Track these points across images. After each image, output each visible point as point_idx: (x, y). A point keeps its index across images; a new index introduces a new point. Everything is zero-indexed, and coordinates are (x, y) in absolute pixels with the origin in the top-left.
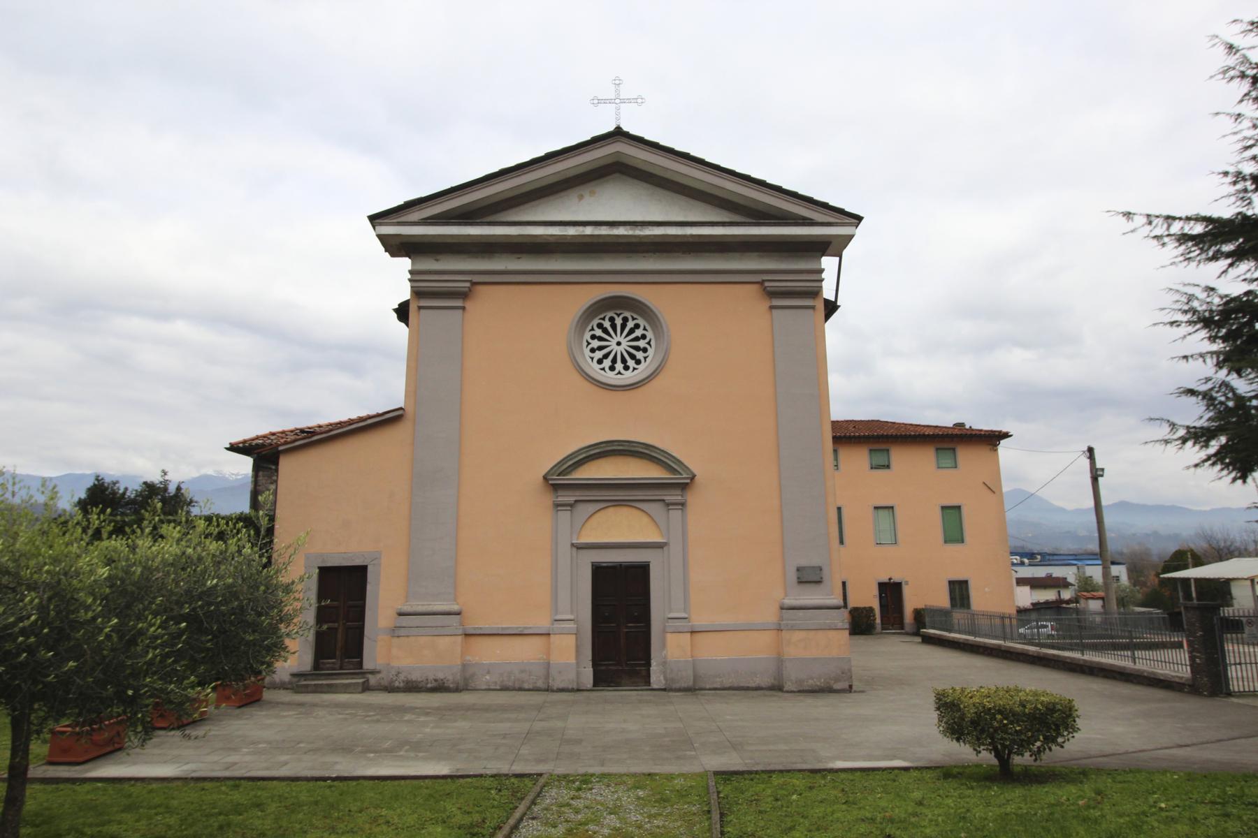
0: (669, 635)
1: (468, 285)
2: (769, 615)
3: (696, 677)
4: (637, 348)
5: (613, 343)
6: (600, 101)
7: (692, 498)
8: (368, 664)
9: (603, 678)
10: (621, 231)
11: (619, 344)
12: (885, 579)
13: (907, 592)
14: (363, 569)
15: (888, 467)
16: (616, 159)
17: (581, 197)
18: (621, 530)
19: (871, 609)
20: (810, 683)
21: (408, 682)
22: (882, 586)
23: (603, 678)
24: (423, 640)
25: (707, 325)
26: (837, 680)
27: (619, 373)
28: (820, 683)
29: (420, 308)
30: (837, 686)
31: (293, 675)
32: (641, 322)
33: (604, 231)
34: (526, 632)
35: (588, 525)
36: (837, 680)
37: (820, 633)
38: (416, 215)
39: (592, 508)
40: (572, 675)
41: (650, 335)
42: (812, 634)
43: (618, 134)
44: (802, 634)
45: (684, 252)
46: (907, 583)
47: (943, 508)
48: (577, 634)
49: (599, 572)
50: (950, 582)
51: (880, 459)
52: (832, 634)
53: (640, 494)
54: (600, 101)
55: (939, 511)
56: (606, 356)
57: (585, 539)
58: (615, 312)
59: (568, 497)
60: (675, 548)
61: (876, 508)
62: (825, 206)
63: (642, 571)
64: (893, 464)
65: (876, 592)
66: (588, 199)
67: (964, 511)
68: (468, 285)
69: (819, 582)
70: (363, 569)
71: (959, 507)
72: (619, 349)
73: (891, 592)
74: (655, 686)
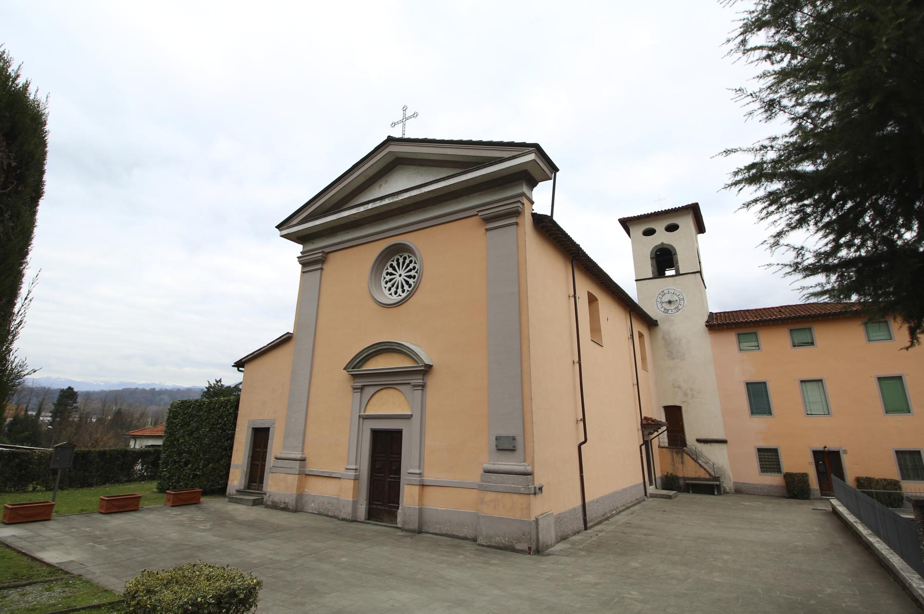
2: (475, 477)
3: (421, 522)
7: (432, 382)
8: (264, 489)
9: (373, 515)
10: (387, 201)
11: (400, 275)
12: (819, 447)
13: (846, 460)
14: (268, 429)
15: (812, 344)
16: (392, 157)
17: (381, 186)
18: (389, 404)
19: (805, 476)
20: (497, 540)
21: (273, 502)
22: (817, 454)
23: (373, 515)
24: (282, 475)
25: (451, 252)
28: (505, 541)
30: (518, 547)
31: (237, 491)
32: (406, 255)
35: (371, 403)
37: (507, 495)
38: (295, 222)
39: (372, 390)
40: (349, 509)
42: (500, 496)
43: (390, 140)
44: (493, 495)
45: (433, 205)
46: (845, 452)
47: (879, 379)
48: (356, 479)
49: (375, 433)
50: (898, 452)
51: (802, 337)
52: (516, 497)
53: (398, 380)
56: (403, 286)
57: (370, 412)
58: (397, 254)
60: (416, 420)
61: (802, 381)
63: (398, 434)
65: (811, 459)
66: (384, 186)
67: (907, 381)
69: (513, 450)
70: (268, 429)
71: (900, 378)
72: (403, 276)
73: (828, 461)
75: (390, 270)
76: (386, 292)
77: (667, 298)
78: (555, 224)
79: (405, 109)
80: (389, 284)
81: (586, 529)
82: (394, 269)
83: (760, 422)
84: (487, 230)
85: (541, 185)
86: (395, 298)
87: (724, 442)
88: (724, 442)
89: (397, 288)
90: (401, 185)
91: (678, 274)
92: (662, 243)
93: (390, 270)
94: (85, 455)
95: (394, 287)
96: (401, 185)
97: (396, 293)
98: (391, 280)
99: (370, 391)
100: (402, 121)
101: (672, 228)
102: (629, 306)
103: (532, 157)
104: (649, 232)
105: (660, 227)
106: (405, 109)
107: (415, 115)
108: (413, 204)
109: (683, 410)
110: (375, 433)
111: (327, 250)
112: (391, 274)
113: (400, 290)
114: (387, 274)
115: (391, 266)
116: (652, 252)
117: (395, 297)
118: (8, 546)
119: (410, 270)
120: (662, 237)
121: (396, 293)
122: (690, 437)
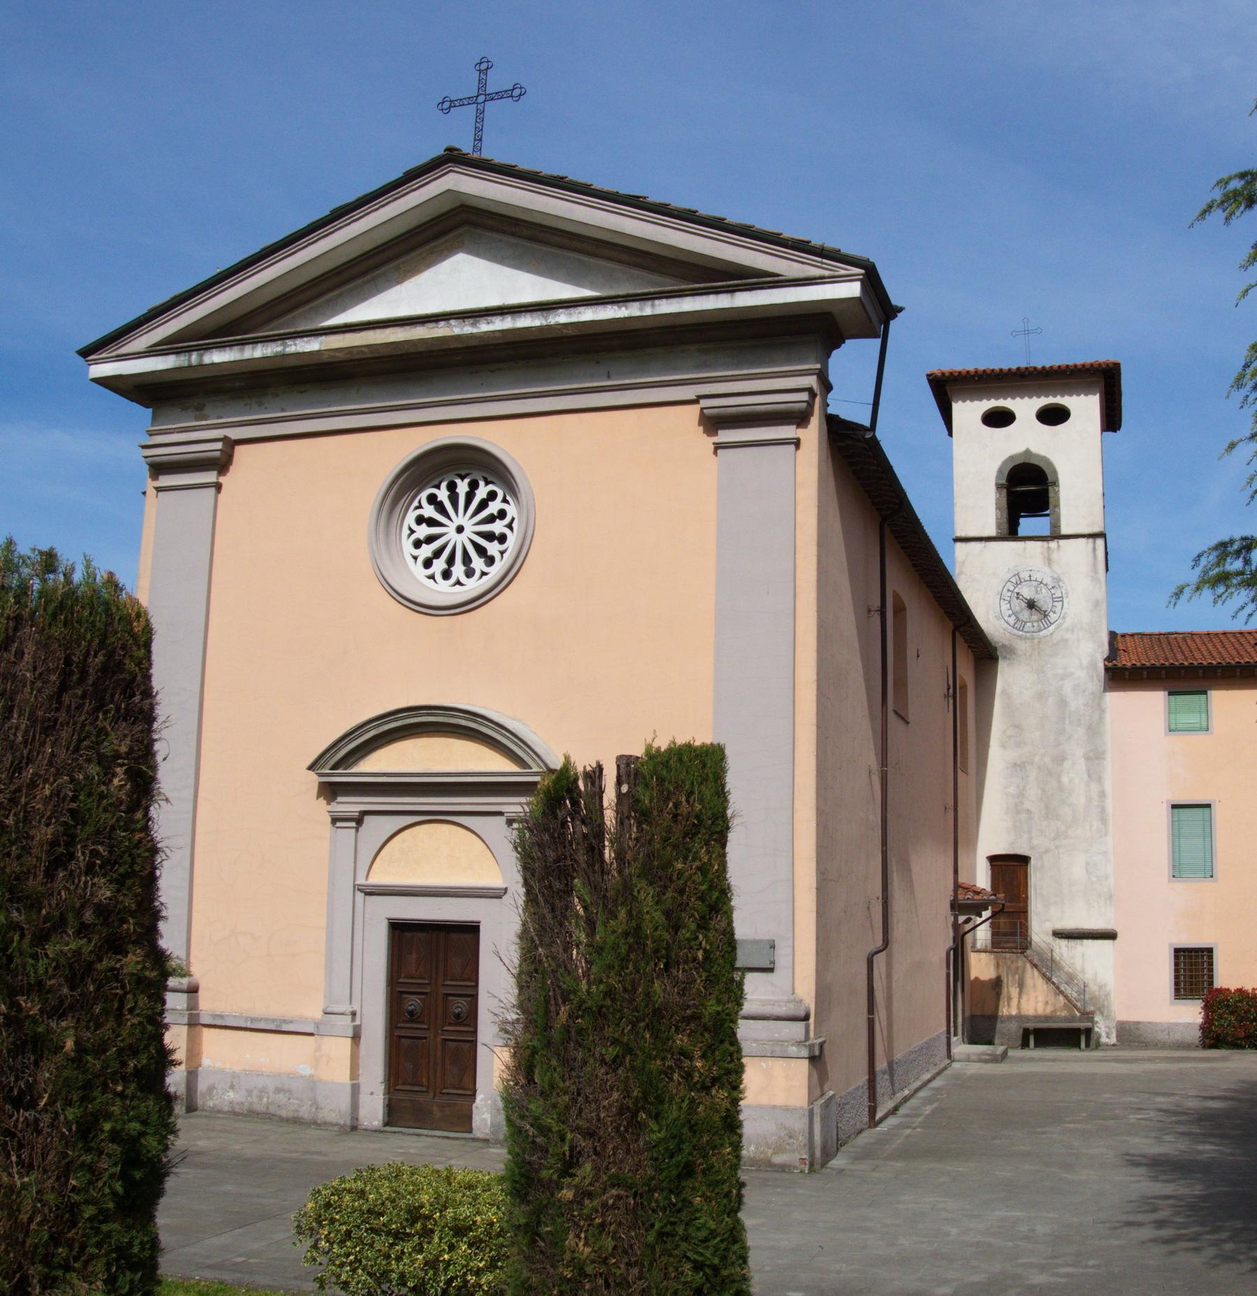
0: (207, 1034)
1: (219, 445)
4: (490, 537)
5: (470, 528)
6: (453, 104)
10: (562, 317)
11: (461, 528)
26: (779, 1150)
27: (458, 583)
29: (159, 489)
33: (466, 329)
34: (285, 1028)
36: (779, 1150)
41: (511, 510)
49: (400, 930)
54: (453, 104)
55: (1162, 816)
57: (379, 877)
59: (350, 805)
62: (802, 247)
64: (1215, 723)
67: (1217, 810)
68: (219, 445)
74: (477, 1133)
75: (429, 511)
76: (419, 571)
77: (1027, 592)
78: (875, 445)
79: (484, 67)
80: (427, 551)
81: (873, 1122)
82: (441, 508)
83: (1185, 893)
84: (718, 447)
85: (850, 344)
86: (444, 592)
87: (1110, 936)
88: (1110, 936)
89: (451, 561)
90: (465, 286)
91: (1056, 535)
92: (1028, 452)
93: (429, 511)
94: (993, 943)
95: (444, 560)
96: (465, 286)
97: (446, 575)
98: (430, 539)
99: (377, 828)
100: (472, 100)
101: (1053, 416)
102: (950, 615)
103: (852, 290)
104: (1000, 419)
105: (1025, 407)
106: (484, 67)
107: (514, 93)
108: (930, 585)
109: (1033, 862)
110: (400, 930)
111: (235, 434)
112: (432, 522)
113: (458, 570)
114: (420, 520)
115: (432, 499)
116: (1000, 471)
117: (444, 586)
118: (267, 1117)
119: (491, 519)
120: (1027, 436)
121: (446, 575)
122: (1040, 928)
